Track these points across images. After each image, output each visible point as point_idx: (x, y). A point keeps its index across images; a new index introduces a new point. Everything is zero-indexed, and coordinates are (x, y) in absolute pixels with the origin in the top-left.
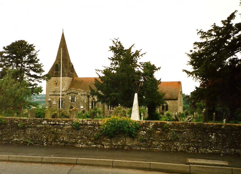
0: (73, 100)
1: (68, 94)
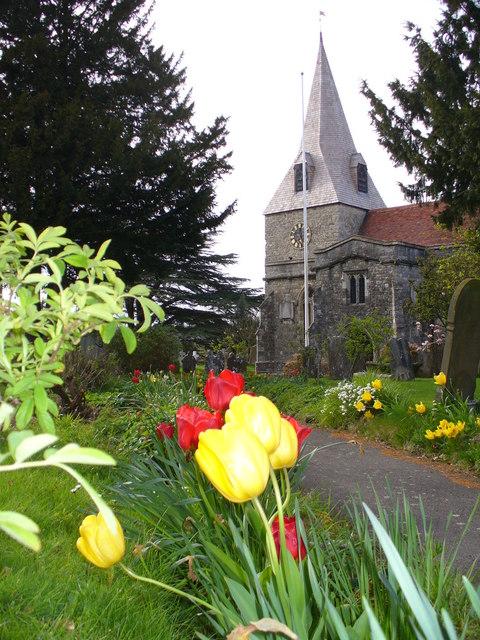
0: (357, 289)
1: (337, 267)
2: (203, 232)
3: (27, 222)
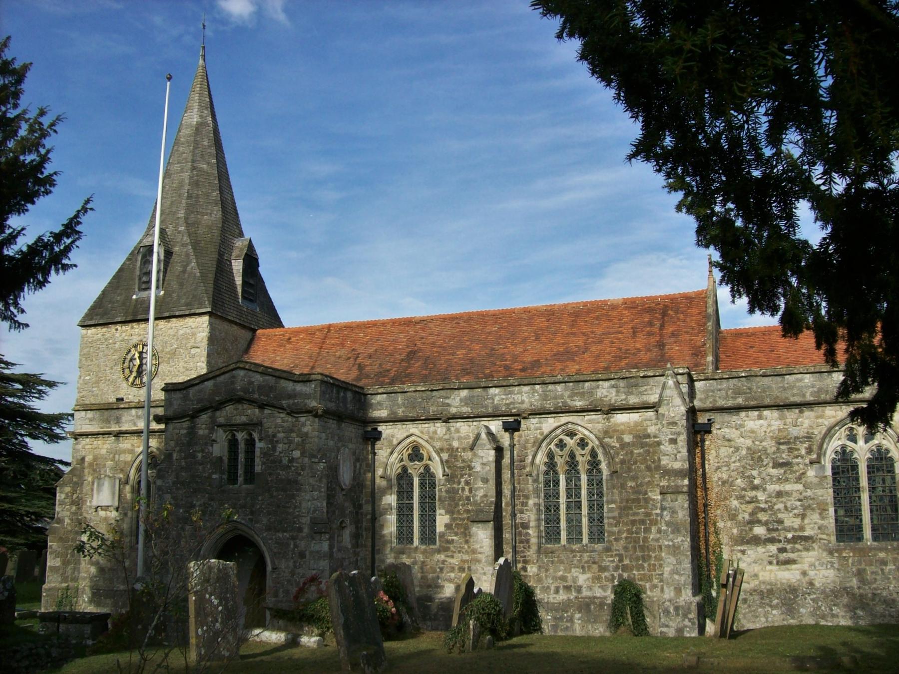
0: (241, 457)
1: (204, 417)
2: (732, 112)
3: (832, 228)
